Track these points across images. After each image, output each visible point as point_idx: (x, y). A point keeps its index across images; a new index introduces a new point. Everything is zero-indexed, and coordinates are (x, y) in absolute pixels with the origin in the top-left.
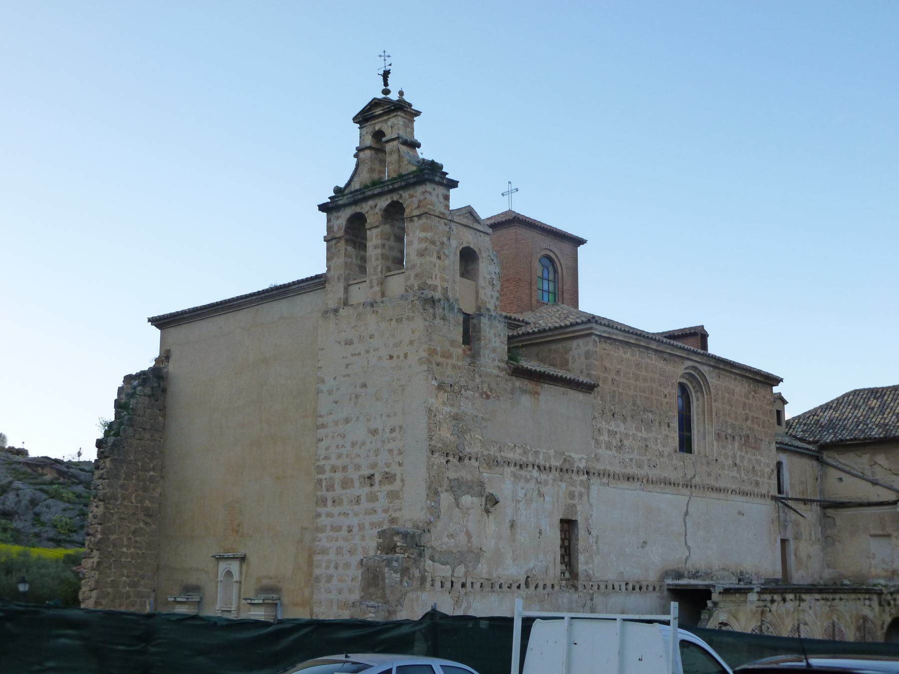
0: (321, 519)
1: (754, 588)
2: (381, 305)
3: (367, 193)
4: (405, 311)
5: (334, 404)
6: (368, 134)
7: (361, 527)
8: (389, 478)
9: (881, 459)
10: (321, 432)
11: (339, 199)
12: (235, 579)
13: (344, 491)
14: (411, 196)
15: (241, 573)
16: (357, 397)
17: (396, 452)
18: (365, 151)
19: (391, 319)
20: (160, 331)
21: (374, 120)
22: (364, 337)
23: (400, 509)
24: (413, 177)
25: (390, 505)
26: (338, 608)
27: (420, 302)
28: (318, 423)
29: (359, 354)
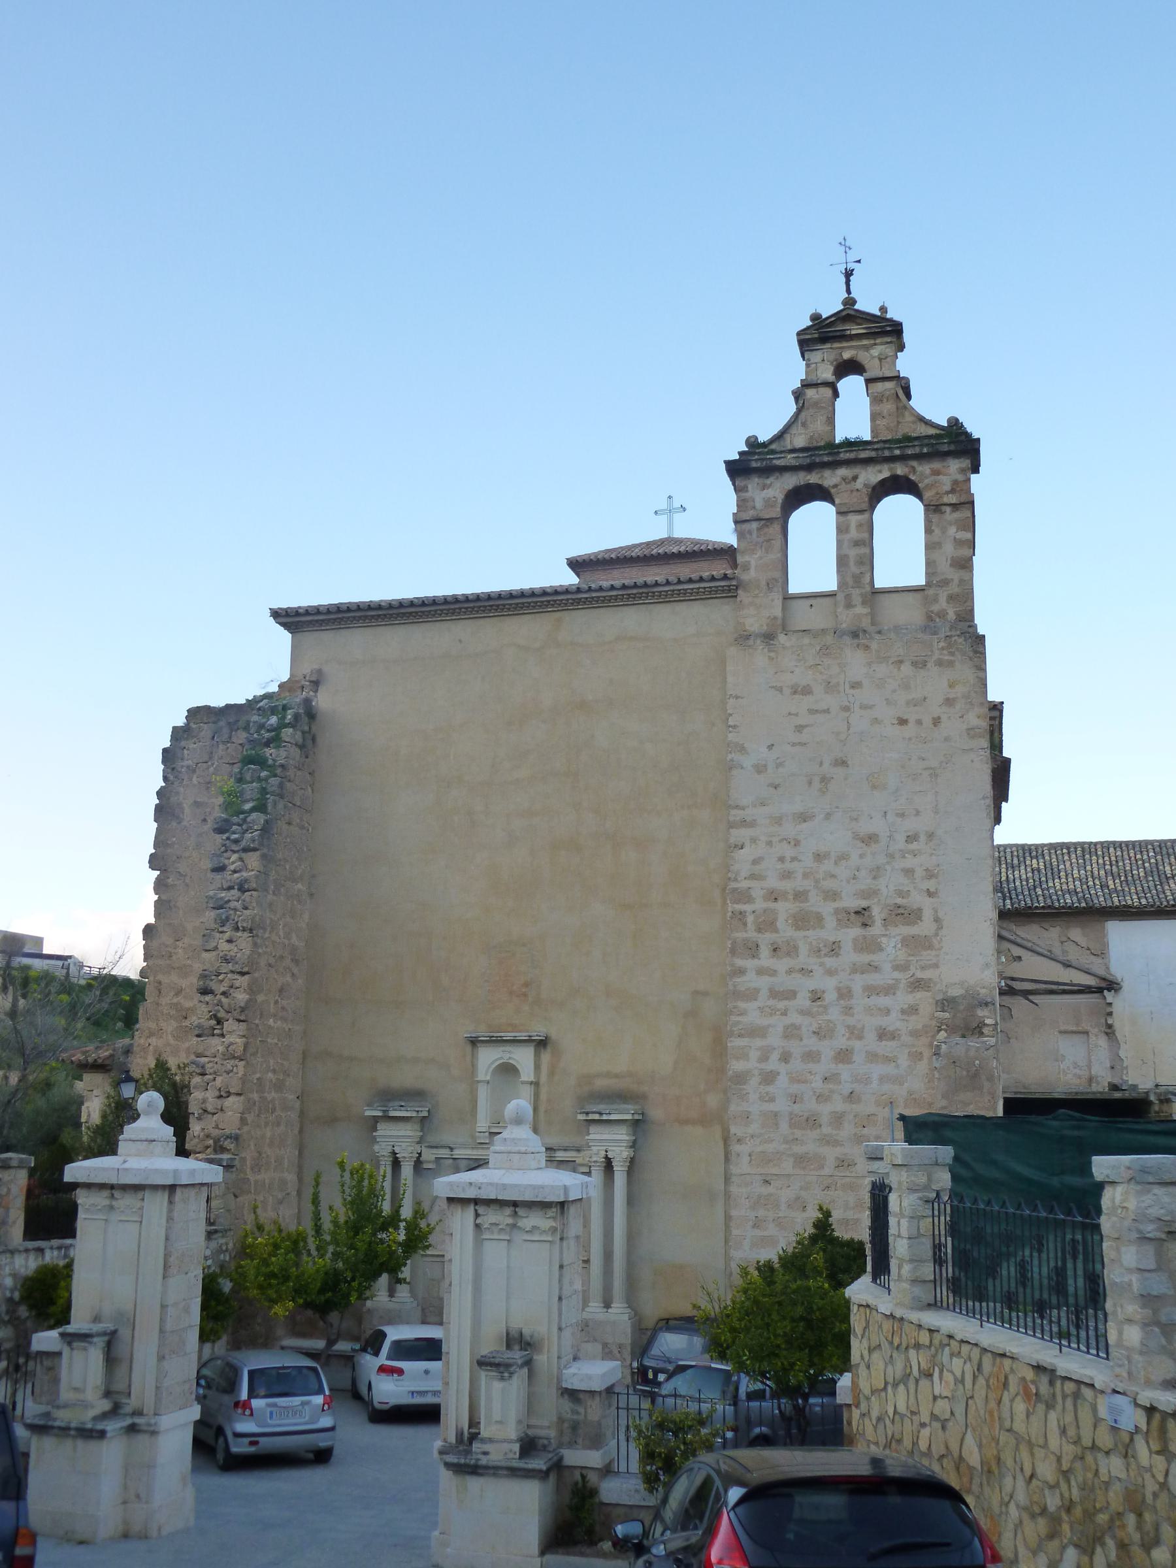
0: (744, 978)
2: (877, 637)
3: (842, 455)
4: (932, 651)
5: (772, 790)
6: (826, 362)
7: (844, 993)
8: (903, 914)
9: (1076, 933)
10: (738, 834)
11: (775, 456)
12: (524, 1078)
13: (801, 933)
14: (936, 473)
15: (537, 1067)
16: (825, 780)
17: (919, 873)
18: (819, 389)
19: (901, 662)
20: (290, 635)
21: (840, 342)
23: (936, 966)
24: (949, 443)
25: (911, 958)
26: (790, 1127)
27: (965, 640)
28: (731, 819)
29: (827, 711)
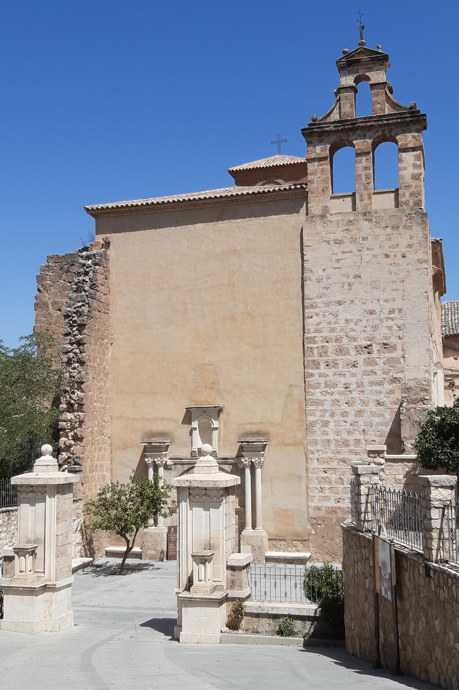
1: (54, 498)
22: (356, 239)
